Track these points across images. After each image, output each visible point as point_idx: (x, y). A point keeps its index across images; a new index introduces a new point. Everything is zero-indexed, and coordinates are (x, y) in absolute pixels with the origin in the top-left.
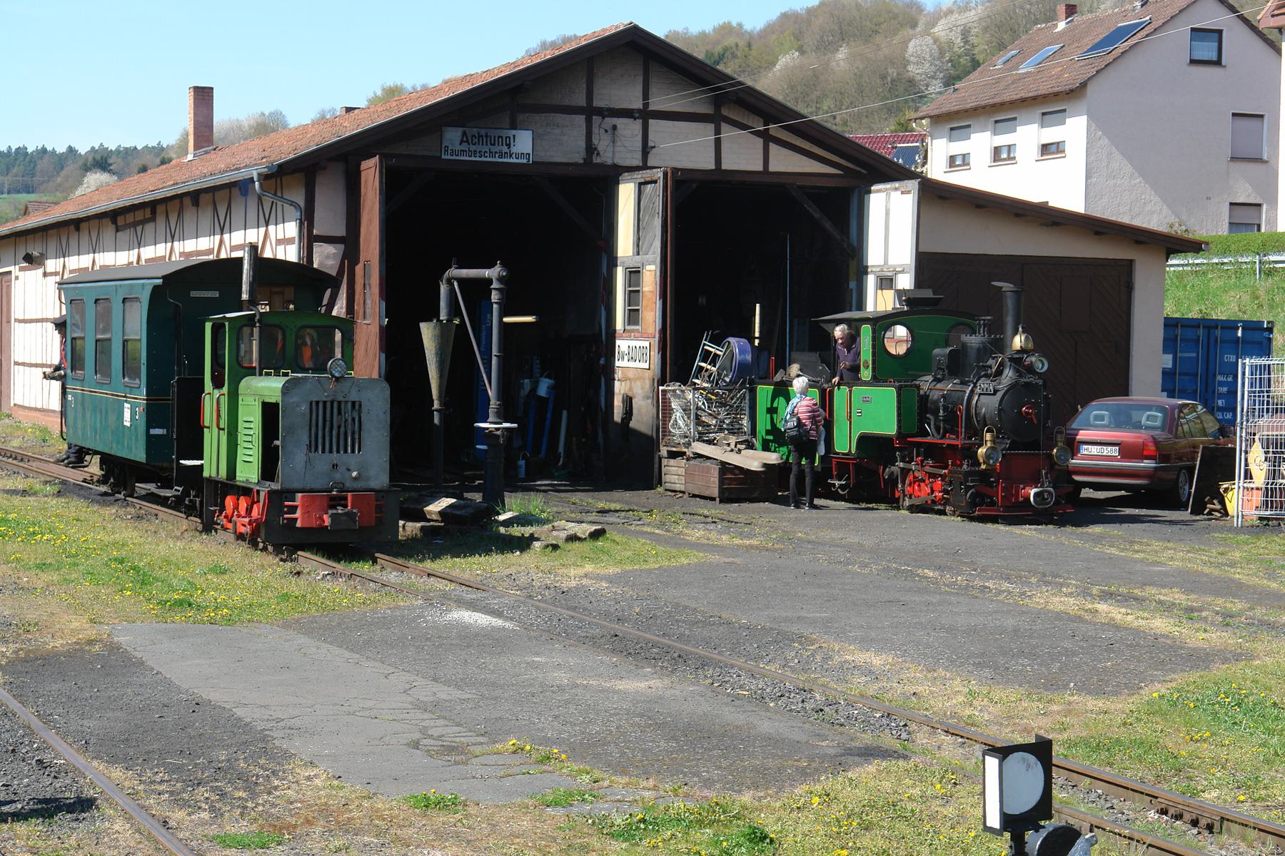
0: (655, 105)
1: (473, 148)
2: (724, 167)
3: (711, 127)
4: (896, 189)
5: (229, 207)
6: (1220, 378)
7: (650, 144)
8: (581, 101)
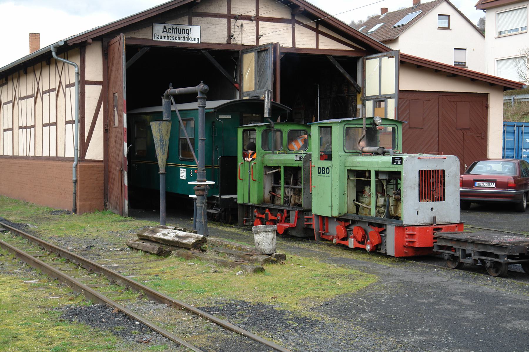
0: (262, 14)
1: (169, 35)
2: (297, 46)
3: (290, 25)
4: (385, 56)
5: (41, 71)
6: (524, 150)
7: (260, 34)
8: (225, 12)
